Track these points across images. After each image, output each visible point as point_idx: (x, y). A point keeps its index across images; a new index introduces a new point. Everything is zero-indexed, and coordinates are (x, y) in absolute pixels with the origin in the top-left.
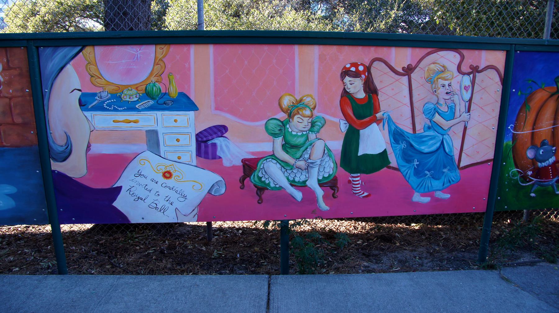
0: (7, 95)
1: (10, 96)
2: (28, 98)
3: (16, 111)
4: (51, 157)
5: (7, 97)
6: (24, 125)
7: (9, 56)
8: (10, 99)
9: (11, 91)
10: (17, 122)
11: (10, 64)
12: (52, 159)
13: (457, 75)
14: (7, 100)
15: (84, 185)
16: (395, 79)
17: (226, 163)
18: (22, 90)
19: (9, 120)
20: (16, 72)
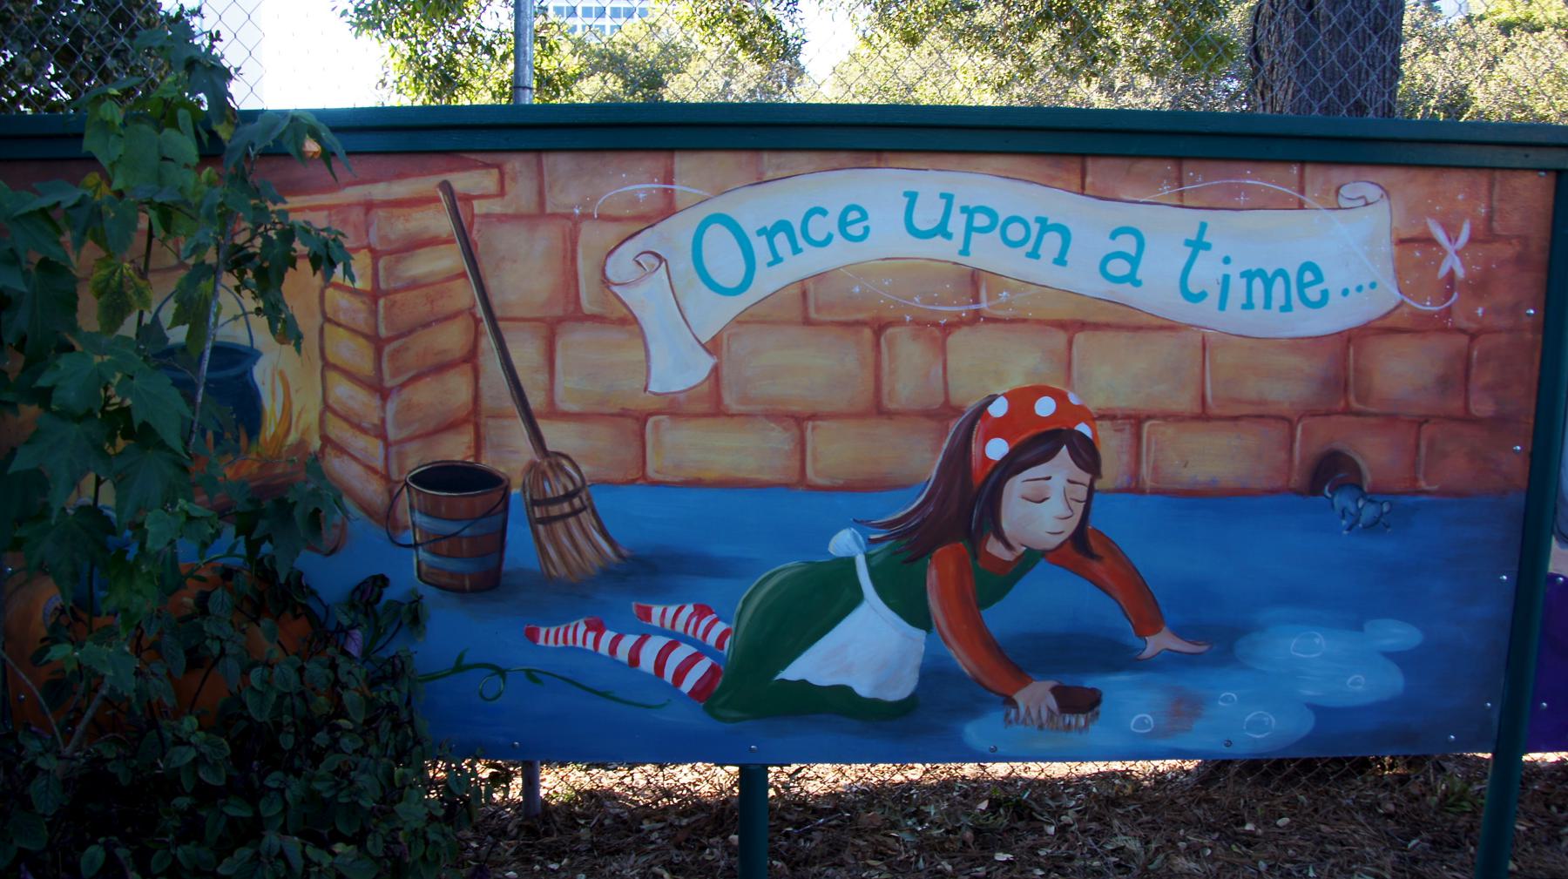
0: (1465, 324)
1: (1473, 326)
2: (1528, 336)
3: (1482, 377)
4: (1556, 529)
5: (1463, 331)
6: (1498, 423)
7: (1496, 197)
8: (1473, 336)
9: (1480, 311)
10: (1477, 414)
11: (1495, 224)
12: (1557, 539)
13: (1170, 430)
14: (1463, 340)
15: (363, 108)
16: (387, 466)
17: (716, 360)
18: (1516, 310)
19: (1455, 405)
20: (1508, 251)
